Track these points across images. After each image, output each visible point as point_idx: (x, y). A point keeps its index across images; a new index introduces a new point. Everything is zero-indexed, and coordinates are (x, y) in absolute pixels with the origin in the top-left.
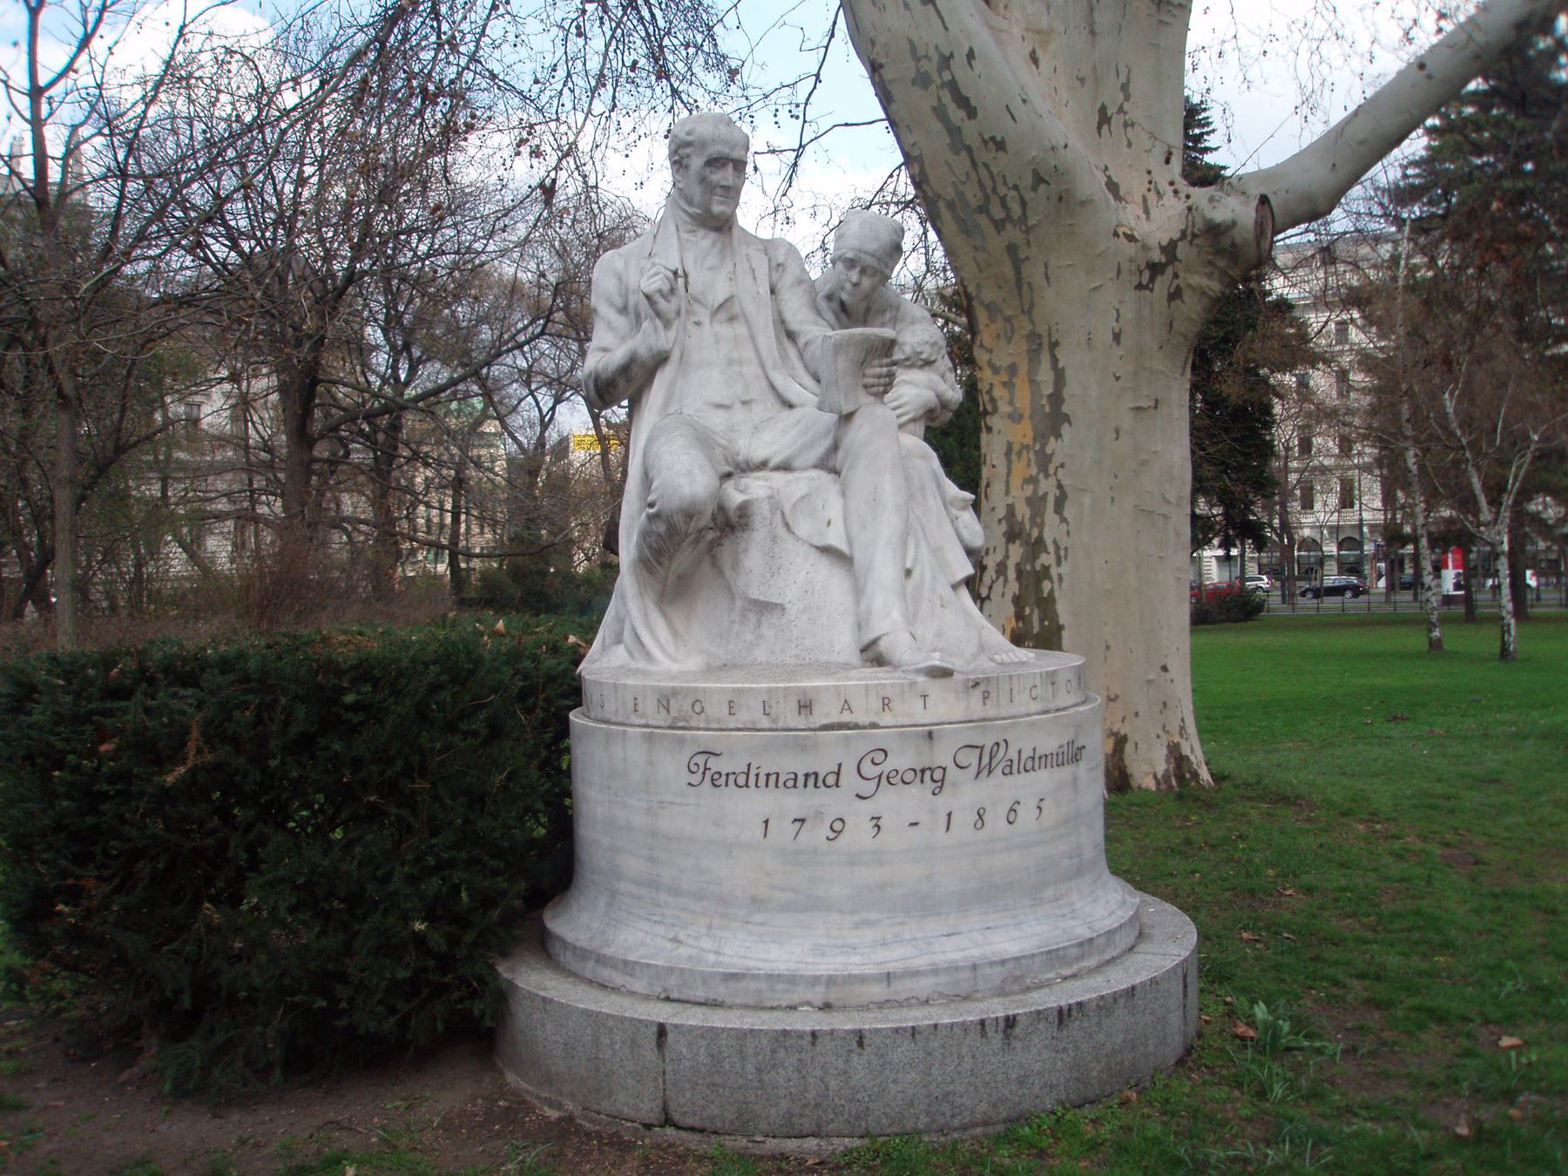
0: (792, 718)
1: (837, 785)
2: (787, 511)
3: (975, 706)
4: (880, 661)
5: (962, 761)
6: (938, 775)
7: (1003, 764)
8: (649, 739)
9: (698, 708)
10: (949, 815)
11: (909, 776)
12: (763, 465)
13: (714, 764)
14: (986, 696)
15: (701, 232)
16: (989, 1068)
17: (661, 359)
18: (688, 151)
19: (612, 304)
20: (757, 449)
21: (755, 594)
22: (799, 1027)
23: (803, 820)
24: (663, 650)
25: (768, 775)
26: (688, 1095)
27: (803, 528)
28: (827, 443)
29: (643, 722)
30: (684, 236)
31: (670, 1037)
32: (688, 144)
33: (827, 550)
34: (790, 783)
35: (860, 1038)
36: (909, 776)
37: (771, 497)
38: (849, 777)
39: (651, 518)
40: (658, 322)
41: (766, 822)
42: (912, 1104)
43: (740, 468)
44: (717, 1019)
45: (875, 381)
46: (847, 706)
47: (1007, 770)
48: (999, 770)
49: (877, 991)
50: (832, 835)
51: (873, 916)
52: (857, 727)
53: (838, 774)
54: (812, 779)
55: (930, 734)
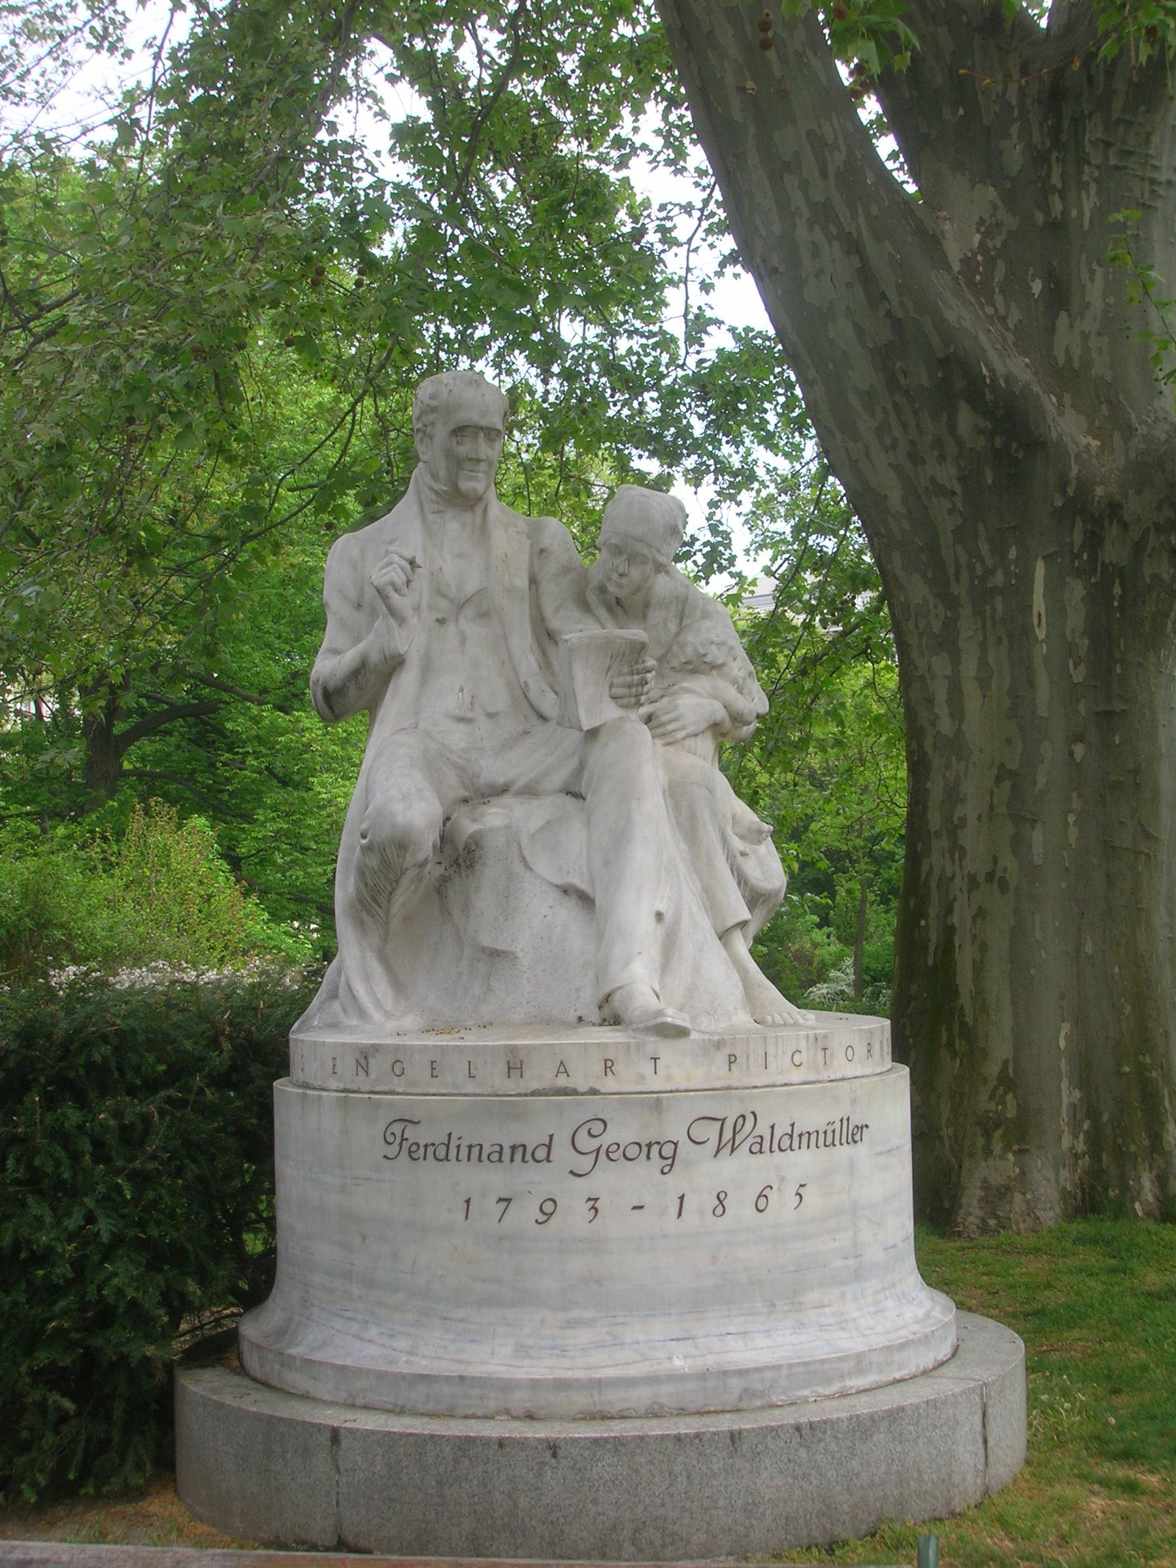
0: (496, 1079)
1: (548, 1160)
2: (524, 841)
3: (715, 1072)
4: (615, 1021)
5: (698, 1132)
6: (668, 1150)
7: (750, 1140)
8: (344, 1104)
9: (398, 1071)
10: (682, 1198)
11: (632, 1151)
12: (504, 790)
13: (411, 1133)
14: (732, 1060)
15: (449, 514)
16: (708, 1492)
17: (394, 664)
18: (431, 417)
19: (346, 598)
20: (493, 770)
21: (486, 941)
22: (486, 1433)
23: (508, 1200)
24: (378, 1004)
25: (470, 1147)
26: (363, 1511)
27: (543, 866)
28: (574, 763)
29: (341, 1086)
30: (430, 517)
31: (344, 1444)
32: (433, 410)
33: (566, 890)
34: (495, 1157)
35: (553, 1448)
36: (632, 1151)
37: (506, 827)
38: (562, 1151)
39: (367, 849)
40: (392, 621)
41: (468, 1201)
42: (614, 1529)
43: (486, 793)
44: (398, 1425)
45: (625, 691)
46: (563, 1068)
47: (756, 1148)
48: (745, 1147)
49: (581, 1401)
50: (542, 1218)
51: (589, 1314)
52: (575, 1092)
53: (549, 1147)
54: (520, 1152)
55: (658, 1102)
